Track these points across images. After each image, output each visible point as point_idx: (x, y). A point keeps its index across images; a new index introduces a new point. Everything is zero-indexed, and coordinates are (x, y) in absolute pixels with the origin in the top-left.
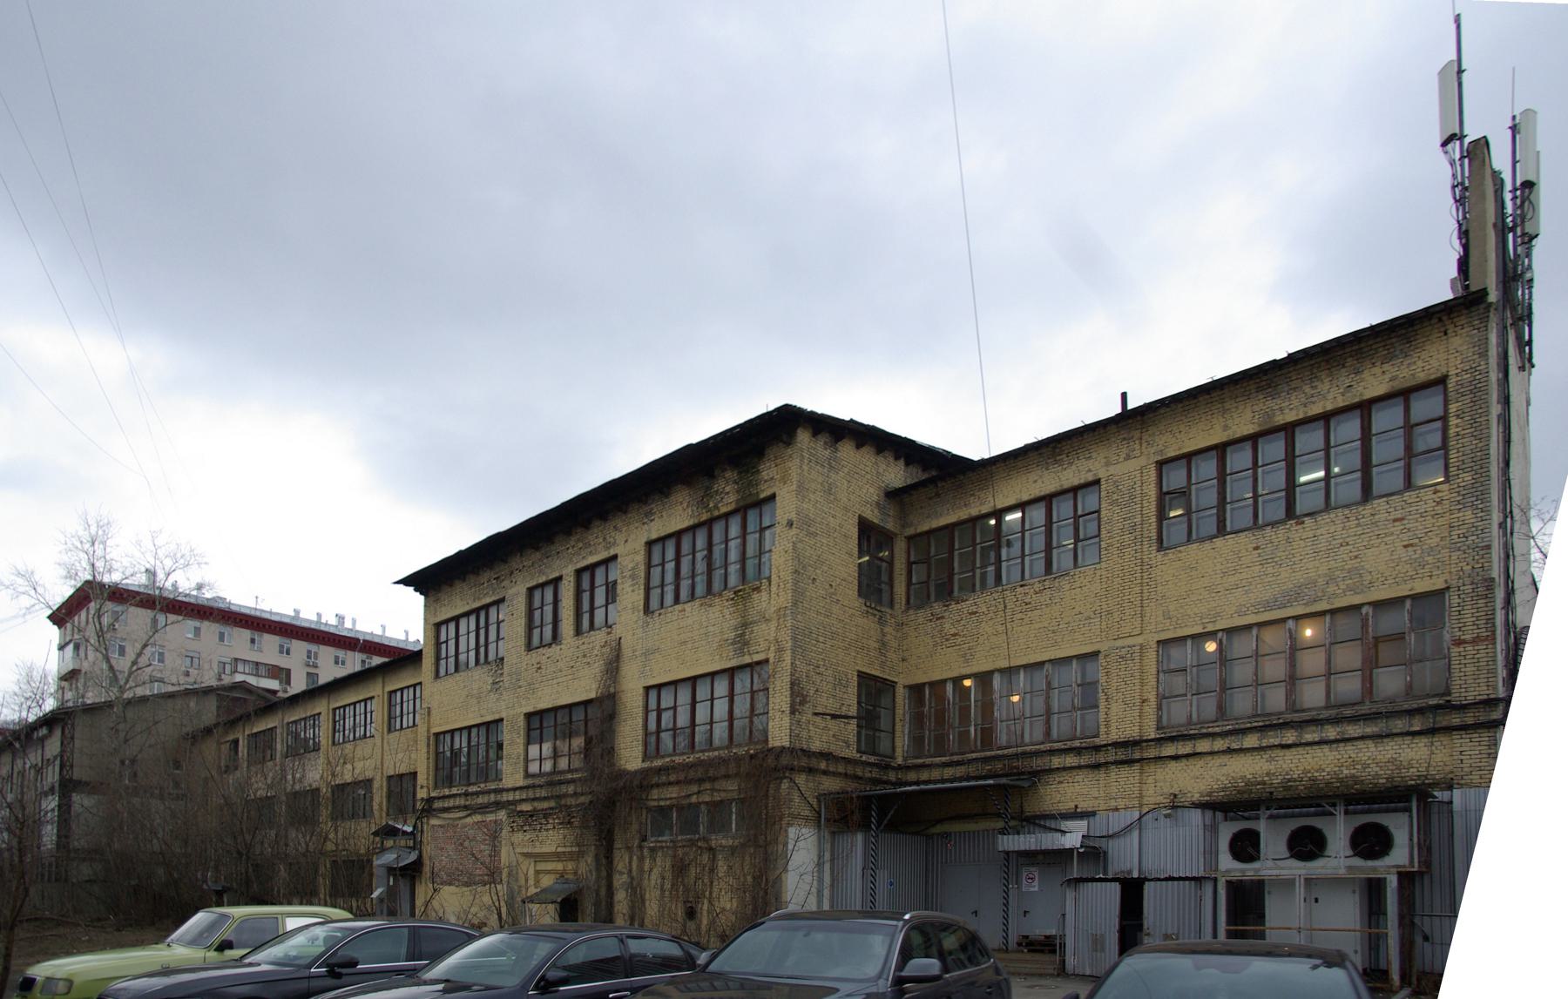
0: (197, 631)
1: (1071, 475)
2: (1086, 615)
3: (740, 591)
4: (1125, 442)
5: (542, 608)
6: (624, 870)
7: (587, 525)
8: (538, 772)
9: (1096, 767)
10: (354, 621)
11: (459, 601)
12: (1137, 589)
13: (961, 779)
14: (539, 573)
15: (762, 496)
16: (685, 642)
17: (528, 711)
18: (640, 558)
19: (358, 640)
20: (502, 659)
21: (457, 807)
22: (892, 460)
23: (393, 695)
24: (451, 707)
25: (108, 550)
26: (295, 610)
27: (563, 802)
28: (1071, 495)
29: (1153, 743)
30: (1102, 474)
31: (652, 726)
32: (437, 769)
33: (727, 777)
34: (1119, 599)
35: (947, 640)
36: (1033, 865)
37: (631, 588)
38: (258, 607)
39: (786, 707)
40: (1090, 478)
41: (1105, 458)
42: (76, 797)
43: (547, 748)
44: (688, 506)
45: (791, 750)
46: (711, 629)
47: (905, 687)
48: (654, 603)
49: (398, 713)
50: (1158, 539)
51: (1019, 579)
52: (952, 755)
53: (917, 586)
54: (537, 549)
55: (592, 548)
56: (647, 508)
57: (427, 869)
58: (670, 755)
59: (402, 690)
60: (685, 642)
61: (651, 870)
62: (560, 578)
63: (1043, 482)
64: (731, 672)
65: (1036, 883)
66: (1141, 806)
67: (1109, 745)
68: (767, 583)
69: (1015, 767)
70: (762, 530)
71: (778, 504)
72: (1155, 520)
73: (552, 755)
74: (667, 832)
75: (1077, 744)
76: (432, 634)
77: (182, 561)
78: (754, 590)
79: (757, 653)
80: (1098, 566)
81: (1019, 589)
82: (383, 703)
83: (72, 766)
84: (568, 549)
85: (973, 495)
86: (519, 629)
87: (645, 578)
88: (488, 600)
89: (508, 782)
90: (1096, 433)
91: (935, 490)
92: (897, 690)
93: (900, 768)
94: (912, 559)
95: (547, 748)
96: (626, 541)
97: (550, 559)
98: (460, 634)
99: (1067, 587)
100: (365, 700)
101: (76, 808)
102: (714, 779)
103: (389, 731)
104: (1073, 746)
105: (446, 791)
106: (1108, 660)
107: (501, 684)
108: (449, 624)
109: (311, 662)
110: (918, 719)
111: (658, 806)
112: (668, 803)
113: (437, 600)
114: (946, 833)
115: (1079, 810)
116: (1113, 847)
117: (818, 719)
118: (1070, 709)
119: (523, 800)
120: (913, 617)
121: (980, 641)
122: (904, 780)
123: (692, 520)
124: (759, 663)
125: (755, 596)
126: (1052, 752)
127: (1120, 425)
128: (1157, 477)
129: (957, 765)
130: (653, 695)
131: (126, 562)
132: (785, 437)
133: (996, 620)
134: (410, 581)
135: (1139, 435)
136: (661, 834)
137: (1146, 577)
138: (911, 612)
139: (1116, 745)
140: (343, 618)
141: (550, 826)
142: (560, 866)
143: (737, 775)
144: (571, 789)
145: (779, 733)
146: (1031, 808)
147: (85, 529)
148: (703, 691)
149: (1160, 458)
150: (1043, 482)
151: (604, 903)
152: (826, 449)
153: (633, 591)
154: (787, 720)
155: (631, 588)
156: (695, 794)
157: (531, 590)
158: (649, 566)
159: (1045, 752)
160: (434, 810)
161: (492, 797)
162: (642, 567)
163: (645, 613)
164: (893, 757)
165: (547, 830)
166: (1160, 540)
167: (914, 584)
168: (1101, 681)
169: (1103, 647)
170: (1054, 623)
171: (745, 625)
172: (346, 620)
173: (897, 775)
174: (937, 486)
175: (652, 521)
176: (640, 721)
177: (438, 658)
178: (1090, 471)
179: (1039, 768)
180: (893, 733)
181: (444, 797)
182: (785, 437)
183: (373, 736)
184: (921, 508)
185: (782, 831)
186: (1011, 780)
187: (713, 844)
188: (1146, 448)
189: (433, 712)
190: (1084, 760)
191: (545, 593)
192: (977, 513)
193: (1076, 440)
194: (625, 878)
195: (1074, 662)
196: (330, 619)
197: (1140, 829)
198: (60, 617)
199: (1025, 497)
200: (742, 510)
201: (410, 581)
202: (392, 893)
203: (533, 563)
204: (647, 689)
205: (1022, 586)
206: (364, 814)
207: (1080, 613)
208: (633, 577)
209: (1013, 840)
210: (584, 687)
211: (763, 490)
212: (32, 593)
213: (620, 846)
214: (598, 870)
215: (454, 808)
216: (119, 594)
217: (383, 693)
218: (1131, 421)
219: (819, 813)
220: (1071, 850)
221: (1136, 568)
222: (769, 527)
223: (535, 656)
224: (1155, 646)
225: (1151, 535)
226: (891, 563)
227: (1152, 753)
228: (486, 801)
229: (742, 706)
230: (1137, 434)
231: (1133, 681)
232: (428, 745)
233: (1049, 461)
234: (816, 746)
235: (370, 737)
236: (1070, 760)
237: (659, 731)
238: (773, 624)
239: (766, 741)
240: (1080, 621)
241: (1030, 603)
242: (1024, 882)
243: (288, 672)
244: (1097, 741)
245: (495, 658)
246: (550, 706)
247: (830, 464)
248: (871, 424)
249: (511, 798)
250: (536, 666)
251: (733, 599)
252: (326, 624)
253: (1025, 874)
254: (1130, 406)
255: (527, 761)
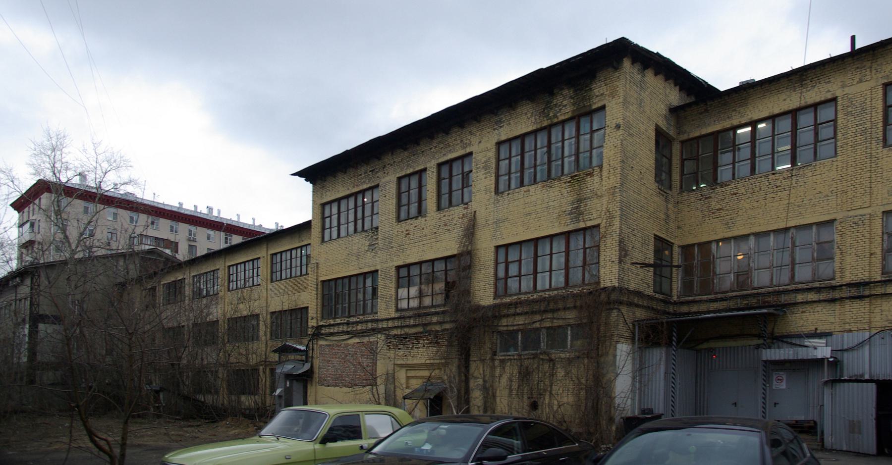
0: (115, 215)
1: (814, 94)
2: (824, 194)
3: (576, 176)
4: (858, 70)
5: (409, 191)
6: (479, 376)
7: (447, 132)
8: (407, 308)
9: (832, 301)
10: (219, 212)
11: (340, 188)
12: (867, 175)
13: (726, 310)
14: (408, 166)
15: (594, 107)
16: (530, 214)
17: (398, 265)
18: (492, 154)
19: (223, 224)
20: (377, 228)
21: (341, 333)
22: (672, 85)
23: (274, 257)
24: (335, 262)
25: (64, 155)
26: (179, 203)
27: (428, 328)
28: (813, 109)
29: (880, 284)
30: (839, 93)
31: (501, 274)
32: (323, 305)
33: (565, 309)
34: (853, 182)
35: (713, 213)
36: (781, 370)
37: (485, 176)
38: (155, 201)
39: (615, 258)
40: (829, 96)
41: (842, 82)
42: (41, 326)
43: (414, 291)
44: (531, 116)
45: (620, 290)
46: (551, 203)
47: (679, 246)
48: (502, 187)
49: (279, 269)
50: (883, 139)
51: (770, 170)
52: (716, 293)
53: (687, 176)
54: (405, 149)
55: (451, 148)
56: (496, 118)
57: (316, 376)
58: (515, 295)
59: (281, 253)
60: (530, 214)
61: (501, 376)
62: (425, 170)
63: (791, 100)
64: (567, 235)
65: (784, 383)
66: (870, 328)
67: (845, 285)
68: (599, 170)
69: (767, 302)
70: (592, 132)
71: (608, 113)
72: (881, 125)
73: (418, 295)
74: (512, 349)
75: (817, 285)
76: (319, 211)
77: (114, 165)
78: (587, 175)
79: (590, 220)
80: (834, 159)
81: (771, 177)
82: (267, 262)
83: (38, 305)
84: (431, 149)
85: (735, 110)
86: (391, 207)
87: (496, 168)
88: (365, 186)
89: (382, 314)
90: (835, 64)
91: (705, 107)
92: (674, 248)
93: (675, 303)
94: (684, 157)
95: (414, 291)
96: (480, 142)
97: (415, 156)
98: (341, 211)
99: (810, 174)
100: (253, 260)
101: (41, 334)
102: (553, 311)
103: (272, 281)
104: (814, 286)
105: (332, 322)
106: (843, 225)
107: (376, 245)
108: (350, 199)
109: (191, 239)
110: (688, 270)
111: (507, 330)
112: (515, 328)
113: (323, 187)
114: (711, 348)
115: (818, 332)
116: (847, 358)
117: (633, 267)
118: (811, 260)
119: (395, 327)
120: (686, 198)
121: (740, 213)
122: (678, 312)
123: (535, 126)
124: (594, 227)
125: (589, 179)
126: (797, 291)
127: (855, 58)
128: (883, 94)
129: (720, 301)
130: (502, 252)
131: (77, 164)
132: (615, 64)
133: (752, 199)
134: (300, 174)
135: (870, 64)
136: (508, 351)
137: (873, 166)
138: (685, 194)
139: (850, 285)
140: (212, 209)
141: (420, 345)
142: (426, 373)
143: (575, 307)
144: (435, 319)
145: (609, 276)
146: (780, 330)
147: (48, 141)
148: (544, 249)
149: (886, 81)
150: (791, 100)
151: (463, 399)
152: (639, 74)
153: (486, 178)
154: (616, 268)
155: (485, 176)
156: (539, 321)
157: (400, 179)
158: (498, 160)
159: (792, 290)
160: (322, 334)
161: (370, 326)
162: (493, 161)
163: (495, 194)
164: (671, 296)
165: (418, 348)
166: (885, 139)
167: (686, 175)
168: (836, 241)
169: (839, 216)
170: (799, 199)
171: (580, 201)
172: (214, 211)
173: (673, 308)
174: (706, 104)
175: (501, 127)
176: (492, 271)
177: (323, 228)
178: (829, 91)
179: (786, 302)
180: (671, 279)
181: (330, 325)
182: (615, 64)
183: (259, 285)
184: (693, 120)
185: (612, 347)
186: (775, 310)
187: (553, 356)
188: (875, 74)
189: (320, 266)
190: (822, 296)
191: (411, 182)
192: (738, 124)
193: (819, 70)
194: (480, 381)
195: (814, 228)
196: (203, 210)
197: (870, 345)
198: (19, 205)
199: (777, 111)
200: (577, 118)
201: (300, 174)
202: (288, 391)
203: (402, 160)
204: (497, 248)
205: (773, 174)
206: (291, 335)
207: (820, 193)
208: (486, 168)
209: (775, 353)
210: (449, 246)
211: (595, 103)
212: (11, 184)
213: (475, 359)
214: (460, 375)
215: (338, 333)
216: (69, 191)
217: (267, 256)
218: (864, 55)
219: (634, 334)
220: (822, 360)
221: (866, 160)
222: (598, 130)
223: (404, 226)
224: (881, 214)
225: (878, 136)
226: (670, 160)
227: (879, 291)
228: (364, 328)
229: (577, 259)
230: (868, 64)
231: (864, 240)
232: (317, 289)
233: (797, 85)
234: (632, 286)
235: (257, 285)
236: (811, 296)
237: (507, 277)
238: (605, 200)
239: (598, 283)
240: (820, 198)
241: (780, 186)
242: (775, 383)
243: (177, 244)
244: (833, 283)
245: (370, 227)
246: (417, 261)
247: (641, 85)
248: (668, 57)
249: (385, 326)
250: (405, 232)
251: (569, 182)
252: (201, 213)
253: (775, 377)
254: (858, 46)
255: (397, 299)
